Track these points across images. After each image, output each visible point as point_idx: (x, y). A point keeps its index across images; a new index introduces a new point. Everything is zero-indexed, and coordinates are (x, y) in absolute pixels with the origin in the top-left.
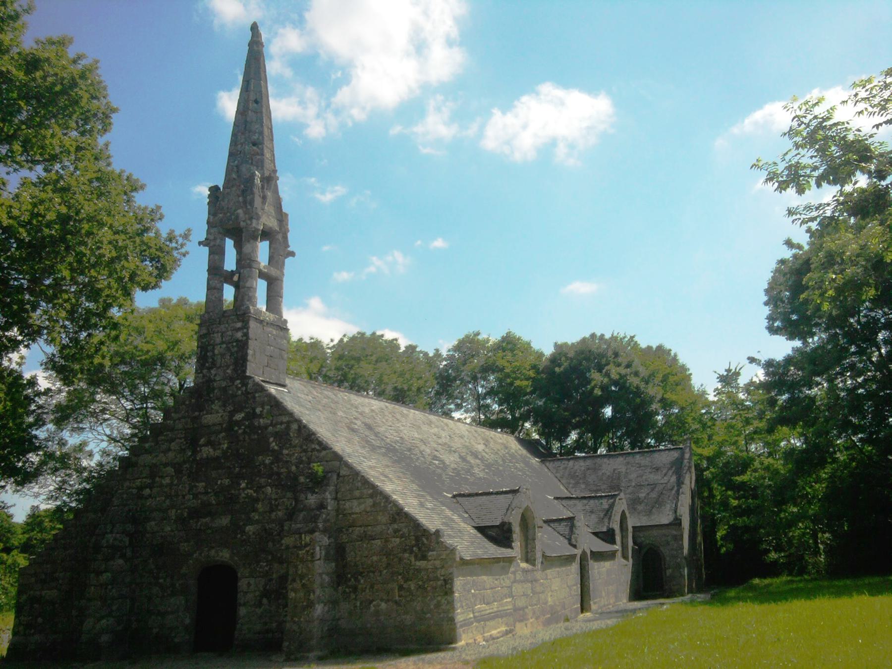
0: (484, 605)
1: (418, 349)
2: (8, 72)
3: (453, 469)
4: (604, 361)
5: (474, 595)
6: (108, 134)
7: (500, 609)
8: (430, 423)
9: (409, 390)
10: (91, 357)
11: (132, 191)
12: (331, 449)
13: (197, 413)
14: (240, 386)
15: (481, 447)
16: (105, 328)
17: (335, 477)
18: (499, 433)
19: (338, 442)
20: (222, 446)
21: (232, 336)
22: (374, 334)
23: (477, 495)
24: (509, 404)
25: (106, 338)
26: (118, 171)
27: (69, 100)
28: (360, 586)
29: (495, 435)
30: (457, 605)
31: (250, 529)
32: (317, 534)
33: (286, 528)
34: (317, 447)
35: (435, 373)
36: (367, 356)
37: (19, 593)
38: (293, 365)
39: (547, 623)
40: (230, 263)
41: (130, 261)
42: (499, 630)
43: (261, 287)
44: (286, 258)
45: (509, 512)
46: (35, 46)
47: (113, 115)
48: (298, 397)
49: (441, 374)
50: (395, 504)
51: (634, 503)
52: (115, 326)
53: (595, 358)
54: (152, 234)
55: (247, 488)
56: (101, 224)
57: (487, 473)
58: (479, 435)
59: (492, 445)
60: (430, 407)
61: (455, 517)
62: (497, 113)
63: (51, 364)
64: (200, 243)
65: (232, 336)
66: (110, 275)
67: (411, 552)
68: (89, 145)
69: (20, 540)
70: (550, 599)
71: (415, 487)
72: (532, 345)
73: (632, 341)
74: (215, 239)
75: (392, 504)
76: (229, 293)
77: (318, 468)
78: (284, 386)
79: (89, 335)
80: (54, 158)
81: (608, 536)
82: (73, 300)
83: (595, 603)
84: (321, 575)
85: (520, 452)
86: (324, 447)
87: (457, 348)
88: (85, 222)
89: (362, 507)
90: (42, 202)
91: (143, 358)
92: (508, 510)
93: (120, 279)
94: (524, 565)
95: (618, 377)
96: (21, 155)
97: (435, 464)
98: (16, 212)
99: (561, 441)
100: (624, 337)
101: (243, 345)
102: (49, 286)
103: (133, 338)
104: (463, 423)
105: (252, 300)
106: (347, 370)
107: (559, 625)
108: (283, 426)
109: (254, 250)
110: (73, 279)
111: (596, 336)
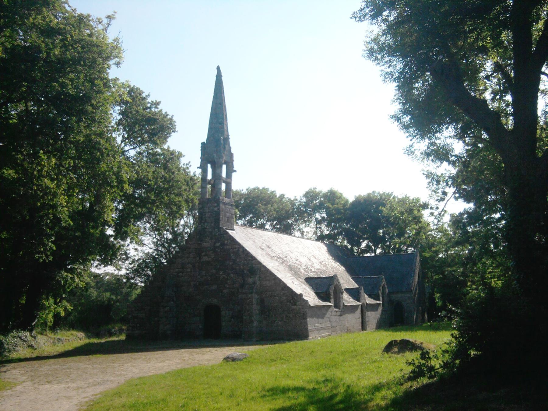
13: (200, 242)
17: (259, 271)
31: (225, 291)
32: (253, 294)
33: (240, 291)
71: (290, 275)
101: (218, 214)
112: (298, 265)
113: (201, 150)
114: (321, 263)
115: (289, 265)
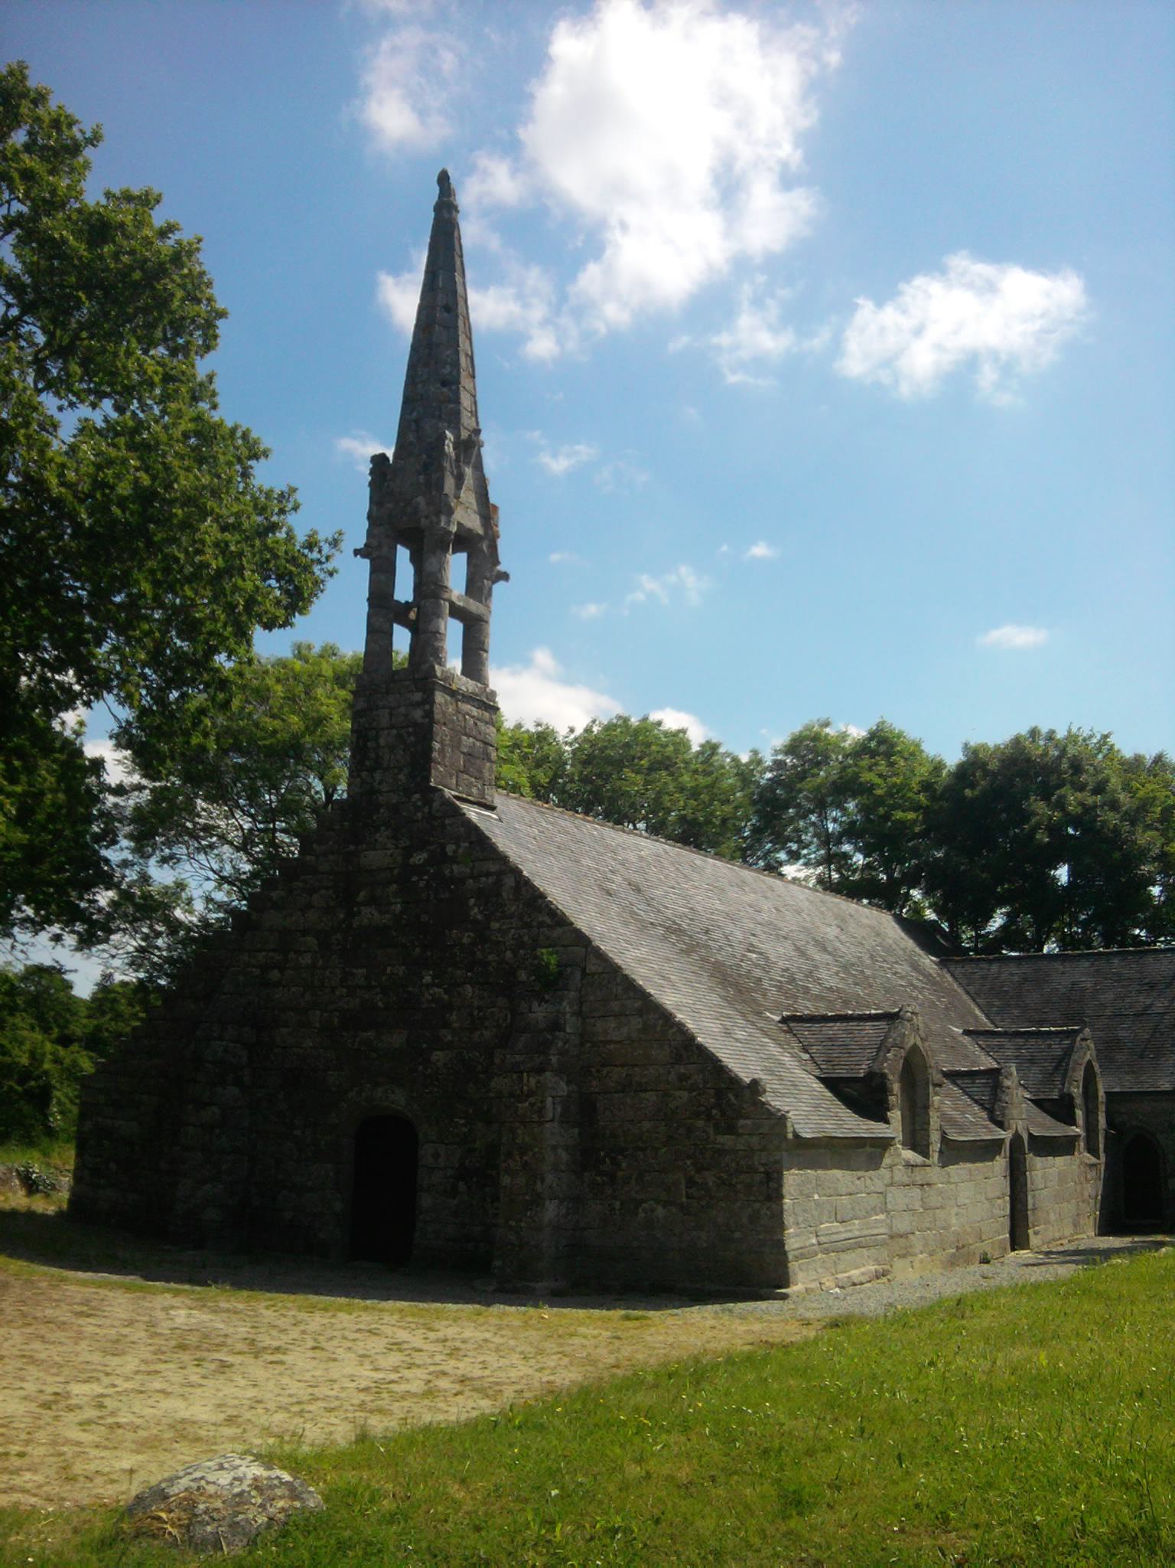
0: (836, 1224)
1: (722, 750)
2: (64, 241)
3: (784, 970)
4: (1054, 779)
5: (817, 1204)
6: (212, 353)
7: (866, 1232)
8: (742, 884)
9: (708, 822)
10: (187, 734)
11: (249, 458)
12: (572, 924)
13: (352, 847)
14: (420, 803)
15: (832, 932)
16: (207, 685)
17: (578, 975)
18: (865, 906)
19: (582, 912)
20: (393, 907)
21: (406, 716)
22: (645, 719)
23: (825, 1019)
24: (882, 855)
25: (210, 703)
26: (229, 424)
27: (154, 298)
28: (620, 1173)
29: (857, 911)
30: (788, 1219)
31: (439, 1056)
32: (548, 1074)
33: (497, 1061)
34: (548, 921)
35: (753, 794)
36: (633, 758)
37: (83, 1116)
38: (507, 771)
39: (952, 1263)
40: (404, 590)
41: (246, 577)
42: (863, 1269)
43: (453, 632)
44: (494, 582)
45: (881, 1054)
46: (104, 201)
47: (219, 323)
48: (515, 828)
49: (761, 795)
50: (680, 1027)
51: (1108, 1048)
52: (223, 684)
53: (1037, 775)
54: (281, 535)
55: (433, 985)
56: (204, 513)
57: (843, 978)
58: (828, 909)
59: (852, 927)
60: (743, 855)
61: (787, 1059)
62: (866, 309)
63: (123, 738)
64: (357, 552)
65: (406, 716)
66: (215, 599)
67: (709, 1118)
68: (183, 373)
69: (85, 1026)
70: (954, 1221)
71: (714, 998)
72: (924, 747)
73: (1105, 743)
74: (380, 546)
75: (675, 1029)
76: (402, 640)
77: (550, 958)
78: (492, 808)
79: (184, 696)
80: (129, 391)
81: (1061, 1110)
82: (157, 634)
83: (1036, 1233)
84: (554, 1148)
85: (903, 944)
86: (560, 920)
87: (792, 748)
88: (178, 505)
89: (625, 1030)
90: (110, 463)
91: (267, 742)
92: (879, 1049)
93: (231, 608)
94: (909, 1155)
95: (1079, 810)
96: (81, 381)
97: (750, 960)
98: (71, 476)
99: (976, 928)
100: (1091, 737)
101: (424, 732)
102: (119, 606)
103: (251, 707)
104: (800, 885)
105: (437, 655)
106: (600, 782)
107: (971, 1268)
108: (491, 880)
109: (442, 567)
110: (157, 598)
111: (1039, 732)
112: (757, 966)
113: (371, 484)
114: (845, 968)
115: (717, 962)
